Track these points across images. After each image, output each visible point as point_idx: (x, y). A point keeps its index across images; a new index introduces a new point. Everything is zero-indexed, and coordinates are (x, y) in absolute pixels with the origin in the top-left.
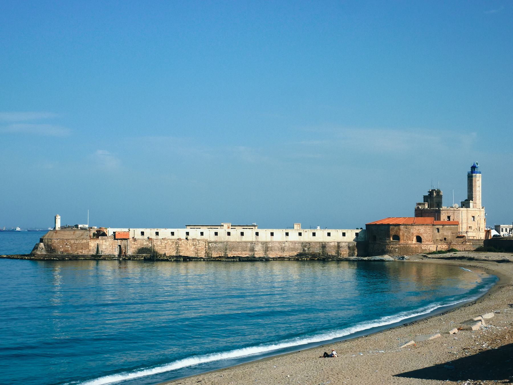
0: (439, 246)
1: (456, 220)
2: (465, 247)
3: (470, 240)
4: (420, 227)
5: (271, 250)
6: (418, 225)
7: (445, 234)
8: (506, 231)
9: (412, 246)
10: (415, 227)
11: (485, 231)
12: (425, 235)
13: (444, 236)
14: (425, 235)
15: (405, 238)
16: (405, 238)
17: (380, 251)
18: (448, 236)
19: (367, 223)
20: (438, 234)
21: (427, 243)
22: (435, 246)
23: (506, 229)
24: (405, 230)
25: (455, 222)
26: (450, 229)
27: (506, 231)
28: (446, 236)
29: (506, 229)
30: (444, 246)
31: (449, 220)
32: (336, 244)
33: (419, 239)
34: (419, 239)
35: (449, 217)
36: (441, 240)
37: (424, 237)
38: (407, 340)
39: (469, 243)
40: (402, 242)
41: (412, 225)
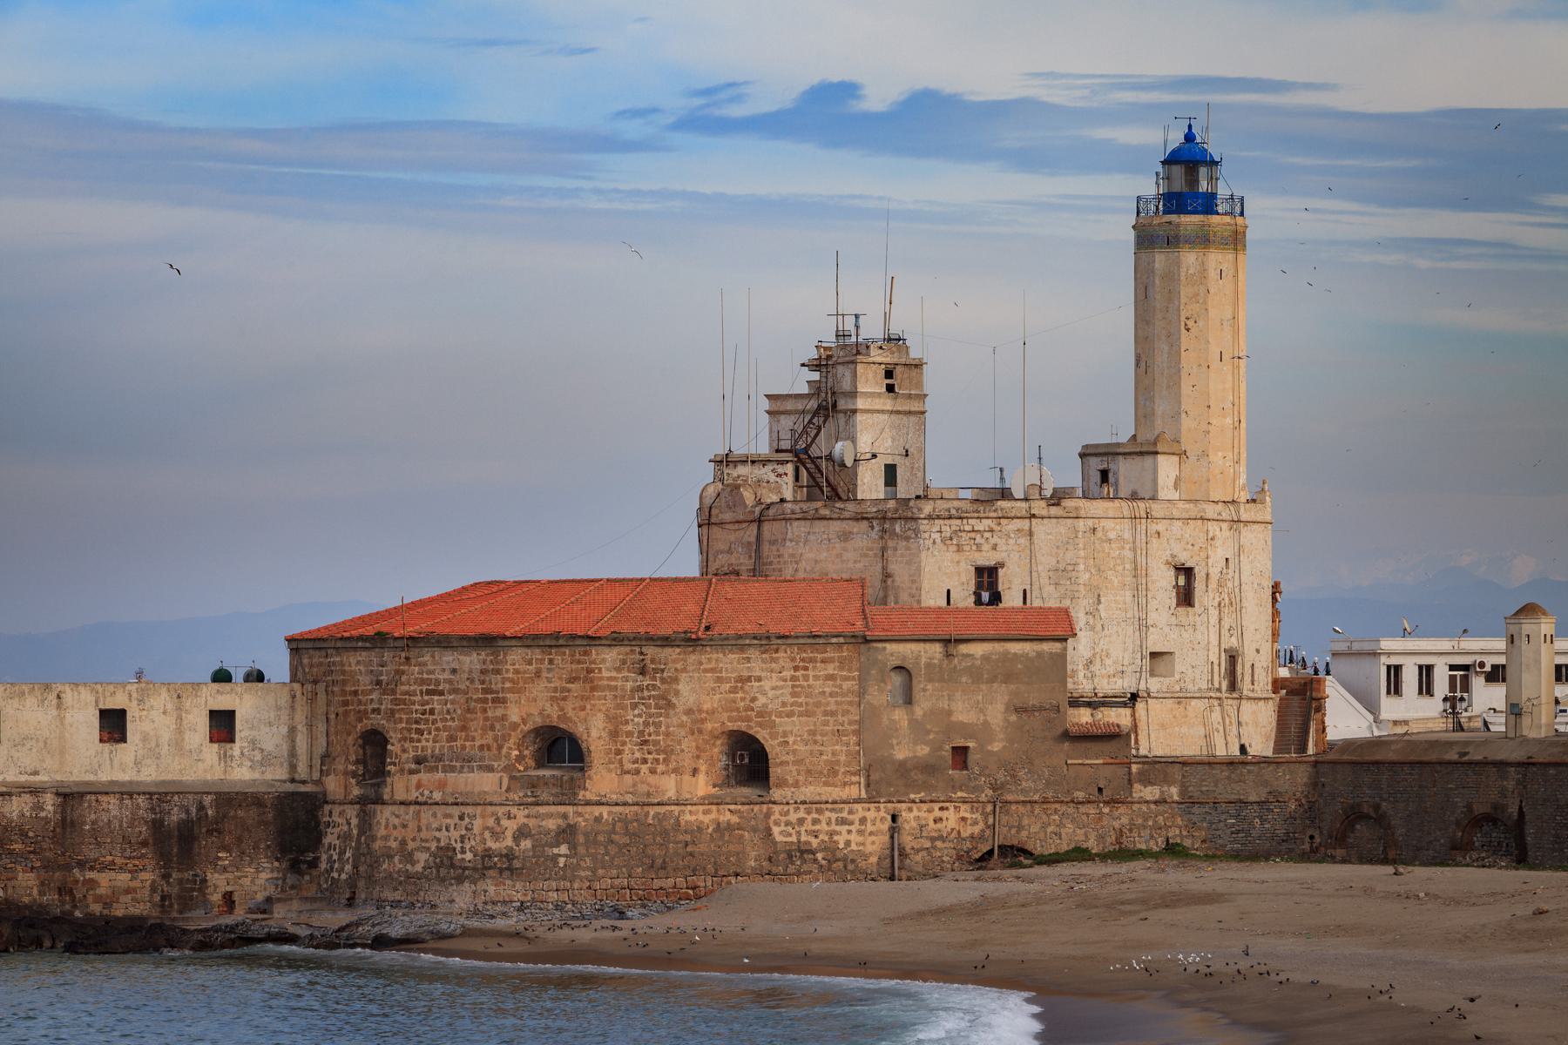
0: (911, 817)
1: (1048, 597)
2: (1122, 816)
3: (1158, 769)
4: (756, 663)
5: (884, 531)
6: (738, 643)
7: (963, 713)
8: (1426, 688)
9: (689, 817)
10: (710, 658)
11: (1277, 684)
12: (795, 726)
13: (951, 728)
14: (795, 726)
15: (631, 752)
16: (631, 752)
17: (422, 857)
18: (983, 731)
19: (297, 629)
20: (900, 715)
21: (809, 792)
22: (877, 817)
23: (1426, 672)
24: (630, 681)
25: (1044, 612)
26: (1005, 672)
27: (1426, 688)
28: (966, 730)
29: (1426, 672)
30: (951, 819)
31: (996, 598)
32: (49, 802)
33: (750, 762)
34: (750, 762)
35: (987, 577)
36: (929, 768)
37: (786, 743)
38: (544, 796)
39: (1151, 793)
40: (602, 781)
41: (690, 642)
